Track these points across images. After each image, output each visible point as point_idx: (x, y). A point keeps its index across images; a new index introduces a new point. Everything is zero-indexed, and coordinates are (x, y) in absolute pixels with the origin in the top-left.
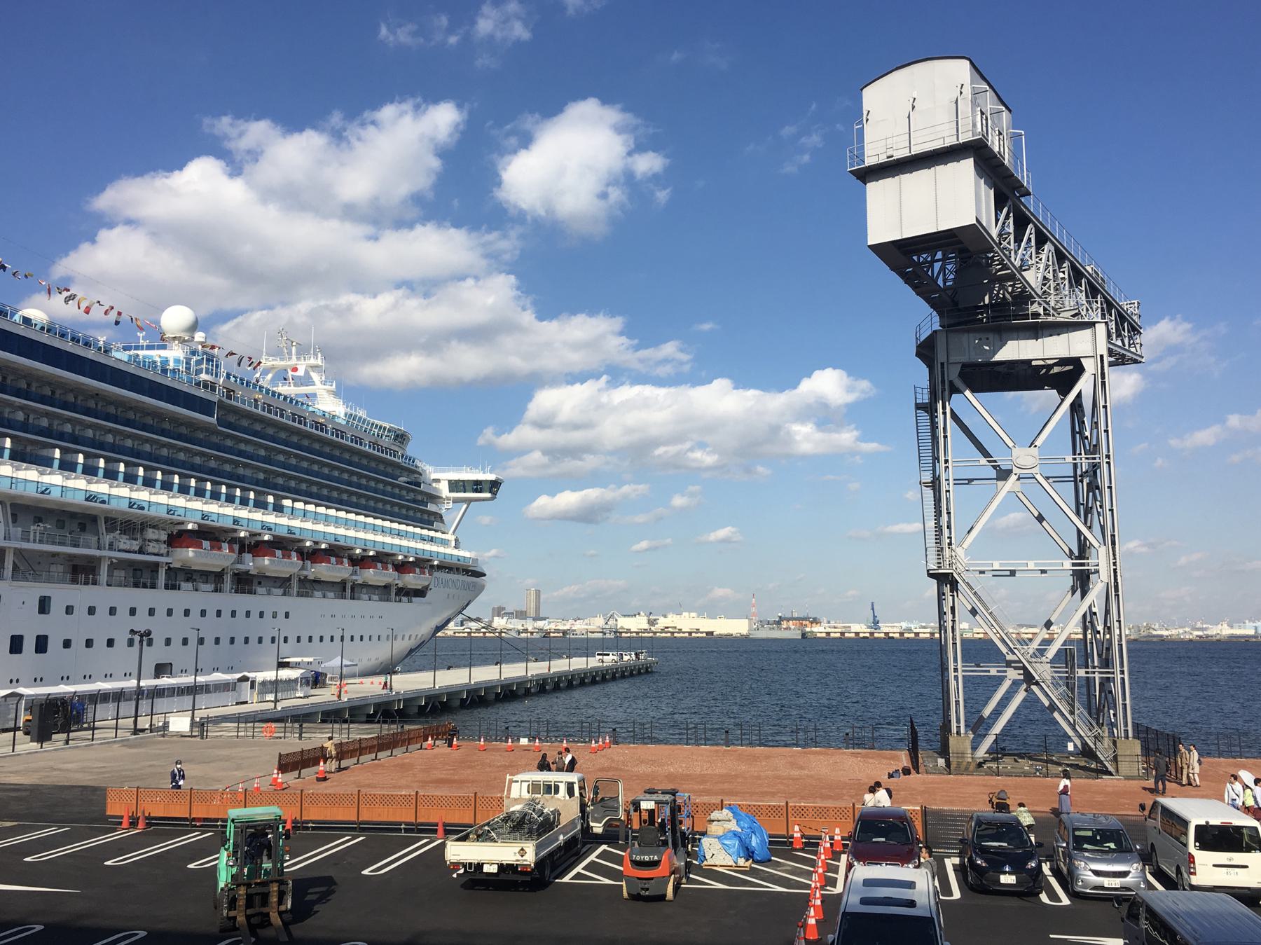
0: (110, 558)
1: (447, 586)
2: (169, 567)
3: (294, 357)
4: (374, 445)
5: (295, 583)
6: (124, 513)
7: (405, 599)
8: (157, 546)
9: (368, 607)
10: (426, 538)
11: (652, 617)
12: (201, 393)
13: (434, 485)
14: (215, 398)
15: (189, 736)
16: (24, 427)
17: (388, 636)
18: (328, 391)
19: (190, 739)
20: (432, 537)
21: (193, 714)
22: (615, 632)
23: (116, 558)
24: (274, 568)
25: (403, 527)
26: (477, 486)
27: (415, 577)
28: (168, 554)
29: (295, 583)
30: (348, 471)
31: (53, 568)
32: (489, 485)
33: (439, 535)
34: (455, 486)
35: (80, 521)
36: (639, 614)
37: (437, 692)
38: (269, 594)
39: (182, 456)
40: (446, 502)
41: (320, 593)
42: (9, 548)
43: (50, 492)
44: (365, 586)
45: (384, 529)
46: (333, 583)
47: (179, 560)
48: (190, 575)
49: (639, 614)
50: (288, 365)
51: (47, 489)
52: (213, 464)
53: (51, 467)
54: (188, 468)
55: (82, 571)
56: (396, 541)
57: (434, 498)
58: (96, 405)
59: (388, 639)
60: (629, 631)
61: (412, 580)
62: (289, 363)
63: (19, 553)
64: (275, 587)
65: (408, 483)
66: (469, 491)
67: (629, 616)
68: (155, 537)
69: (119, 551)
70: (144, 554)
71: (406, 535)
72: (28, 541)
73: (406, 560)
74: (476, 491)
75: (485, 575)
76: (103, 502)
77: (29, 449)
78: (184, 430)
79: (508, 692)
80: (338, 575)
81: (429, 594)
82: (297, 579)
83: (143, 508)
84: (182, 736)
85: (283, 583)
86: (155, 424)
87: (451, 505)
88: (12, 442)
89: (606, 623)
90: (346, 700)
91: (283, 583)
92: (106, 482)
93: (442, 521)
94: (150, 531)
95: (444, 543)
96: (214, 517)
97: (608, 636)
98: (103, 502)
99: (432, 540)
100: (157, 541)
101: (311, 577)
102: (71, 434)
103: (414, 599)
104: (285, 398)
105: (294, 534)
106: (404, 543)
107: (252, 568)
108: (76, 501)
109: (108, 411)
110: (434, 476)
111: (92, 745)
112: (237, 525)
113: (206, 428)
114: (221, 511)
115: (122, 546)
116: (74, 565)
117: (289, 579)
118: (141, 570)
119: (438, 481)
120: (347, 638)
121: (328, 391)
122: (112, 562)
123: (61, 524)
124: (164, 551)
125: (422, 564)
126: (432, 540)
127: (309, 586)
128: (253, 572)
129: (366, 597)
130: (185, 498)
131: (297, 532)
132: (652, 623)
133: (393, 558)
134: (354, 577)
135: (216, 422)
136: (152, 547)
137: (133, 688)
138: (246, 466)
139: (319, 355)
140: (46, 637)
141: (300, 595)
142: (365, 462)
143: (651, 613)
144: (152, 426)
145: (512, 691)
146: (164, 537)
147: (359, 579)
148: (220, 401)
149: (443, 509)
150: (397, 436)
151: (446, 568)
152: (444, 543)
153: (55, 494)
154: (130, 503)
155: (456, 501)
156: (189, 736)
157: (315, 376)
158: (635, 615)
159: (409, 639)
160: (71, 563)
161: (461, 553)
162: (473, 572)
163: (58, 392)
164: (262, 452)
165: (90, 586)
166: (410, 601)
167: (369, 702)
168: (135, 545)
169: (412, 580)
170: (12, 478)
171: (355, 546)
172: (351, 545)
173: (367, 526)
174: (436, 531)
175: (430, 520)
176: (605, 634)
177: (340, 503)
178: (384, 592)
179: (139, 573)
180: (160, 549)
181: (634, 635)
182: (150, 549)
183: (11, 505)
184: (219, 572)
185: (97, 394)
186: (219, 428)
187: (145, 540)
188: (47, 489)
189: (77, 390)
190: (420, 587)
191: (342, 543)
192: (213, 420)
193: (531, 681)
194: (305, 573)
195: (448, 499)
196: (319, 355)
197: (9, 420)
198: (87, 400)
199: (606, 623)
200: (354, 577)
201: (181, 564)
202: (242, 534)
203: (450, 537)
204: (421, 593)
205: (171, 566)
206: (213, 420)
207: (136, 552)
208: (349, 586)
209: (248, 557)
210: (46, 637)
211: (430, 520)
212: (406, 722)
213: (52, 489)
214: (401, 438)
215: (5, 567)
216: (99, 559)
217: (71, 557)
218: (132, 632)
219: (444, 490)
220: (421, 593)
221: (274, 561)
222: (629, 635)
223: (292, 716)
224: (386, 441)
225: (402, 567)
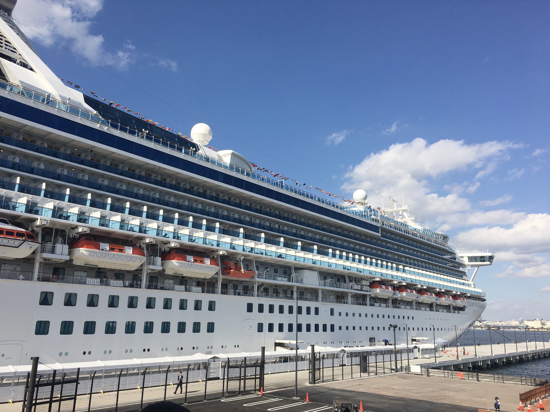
0: (351, 293)
1: (473, 305)
2: (437, 304)
3: (395, 207)
4: (435, 242)
5: (414, 304)
6: (355, 274)
7: (456, 312)
8: (366, 287)
9: (443, 315)
10: (462, 283)
11: (543, 321)
12: (374, 223)
13: (461, 259)
14: (379, 225)
15: (420, 375)
16: (228, 218)
17: (409, 330)
18: (411, 220)
19: (421, 376)
20: (464, 283)
21: (166, 387)
22: (526, 329)
23: (354, 293)
24: (382, 294)
25: (452, 279)
26: (482, 259)
27: (461, 301)
28: (370, 291)
29: (414, 304)
30: (408, 248)
31: (331, 297)
32: (488, 259)
33: (466, 282)
34: (471, 259)
35: (331, 277)
36: (536, 320)
37: (494, 358)
38: (405, 308)
39: (339, 242)
40: (467, 267)
41: (403, 306)
42: (320, 289)
43: (331, 267)
44: (440, 305)
45: (445, 280)
46: (426, 304)
47: (374, 294)
48: (375, 300)
49: (536, 320)
50: (394, 211)
51: (330, 265)
52: (379, 253)
53: (238, 237)
54: (348, 249)
55: (340, 298)
56: (418, 278)
57: (463, 265)
58: (304, 220)
59: (404, 330)
60: (533, 328)
61: (459, 303)
62: (394, 210)
63: (323, 291)
64: (91, 277)
65: (451, 258)
66: (478, 261)
67: (530, 320)
68: (366, 284)
69: (354, 290)
70: (362, 291)
71: (453, 282)
72: (325, 286)
73: (422, 288)
74: (481, 261)
75: (486, 300)
76: (348, 270)
77: (271, 238)
78: (346, 232)
79: (493, 363)
80: (431, 300)
81: (466, 309)
82: (415, 302)
83: (361, 272)
84: (415, 374)
85: (409, 303)
86: (320, 226)
87: (470, 268)
88: (91, 196)
89: (520, 324)
90: (460, 360)
91: (409, 303)
92: (302, 252)
93: (466, 276)
94: (364, 281)
95: (469, 285)
96: (385, 275)
97: (522, 330)
98: (348, 270)
99: (464, 284)
100: (366, 285)
101: (420, 301)
102: (287, 231)
103: (460, 312)
104: (401, 224)
105: (413, 282)
106: (422, 279)
107: (399, 297)
108: (291, 261)
109: (331, 229)
110: (460, 255)
111: (369, 378)
112: (382, 276)
113: (377, 238)
114: (338, 262)
115: (355, 288)
116: (337, 296)
117: (388, 299)
118: (358, 298)
119: (462, 257)
120: (436, 329)
121: (411, 220)
122: (352, 294)
123: (271, 270)
124: (369, 290)
125: (463, 295)
126: (464, 284)
127: (420, 305)
128: (399, 299)
129: (441, 310)
130: (321, 256)
131: (414, 281)
132: (543, 324)
133: (415, 287)
134: (437, 301)
135: (380, 235)
136: (365, 288)
137: (294, 354)
138: (390, 253)
139: (406, 205)
140: (213, 324)
141: (417, 309)
142: (411, 242)
143: (542, 319)
144: (327, 229)
145: (495, 363)
146: (368, 284)
147: (438, 303)
148: (381, 226)
149: (466, 270)
150: (444, 237)
151: (472, 297)
152: (469, 285)
153: (333, 268)
154: (344, 267)
155: (472, 266)
156: (420, 375)
157: (405, 214)
158: (534, 320)
159: (460, 330)
160: (336, 295)
161: (476, 290)
162: (480, 298)
163: (263, 208)
164: (396, 247)
165: (346, 304)
166: (459, 313)
167: (469, 361)
168: (359, 287)
169: (459, 303)
170: (266, 250)
171: (436, 287)
172: (434, 287)
173: (411, 272)
174: (465, 280)
175: (461, 275)
176: (482, 328)
177: (426, 268)
178: (448, 308)
179: (358, 299)
180: (367, 289)
181: (536, 330)
182: (364, 289)
183: (294, 267)
184: (212, 279)
185: (341, 227)
186: (381, 238)
187: (362, 285)
188: (330, 265)
189: (250, 199)
190: (462, 306)
191: (431, 286)
192: (379, 235)
193: (530, 353)
194: (395, 296)
195: (469, 265)
196: (406, 205)
197: (314, 238)
198: (337, 229)
199: (520, 324)
200: (437, 301)
201: (374, 295)
202: (395, 282)
203: (470, 282)
204: (462, 309)
205: (372, 296)
206: (379, 235)
207: (359, 290)
208: (434, 305)
209: (397, 292)
210: (213, 324)
211: (461, 275)
212: (479, 372)
213: (332, 265)
214: (445, 238)
215: (294, 294)
216: (347, 294)
217: (338, 292)
218: (391, 325)
219: (466, 261)
220: (462, 309)
221: (408, 294)
222: (533, 330)
223: (443, 367)
224: (440, 240)
225: (455, 297)
